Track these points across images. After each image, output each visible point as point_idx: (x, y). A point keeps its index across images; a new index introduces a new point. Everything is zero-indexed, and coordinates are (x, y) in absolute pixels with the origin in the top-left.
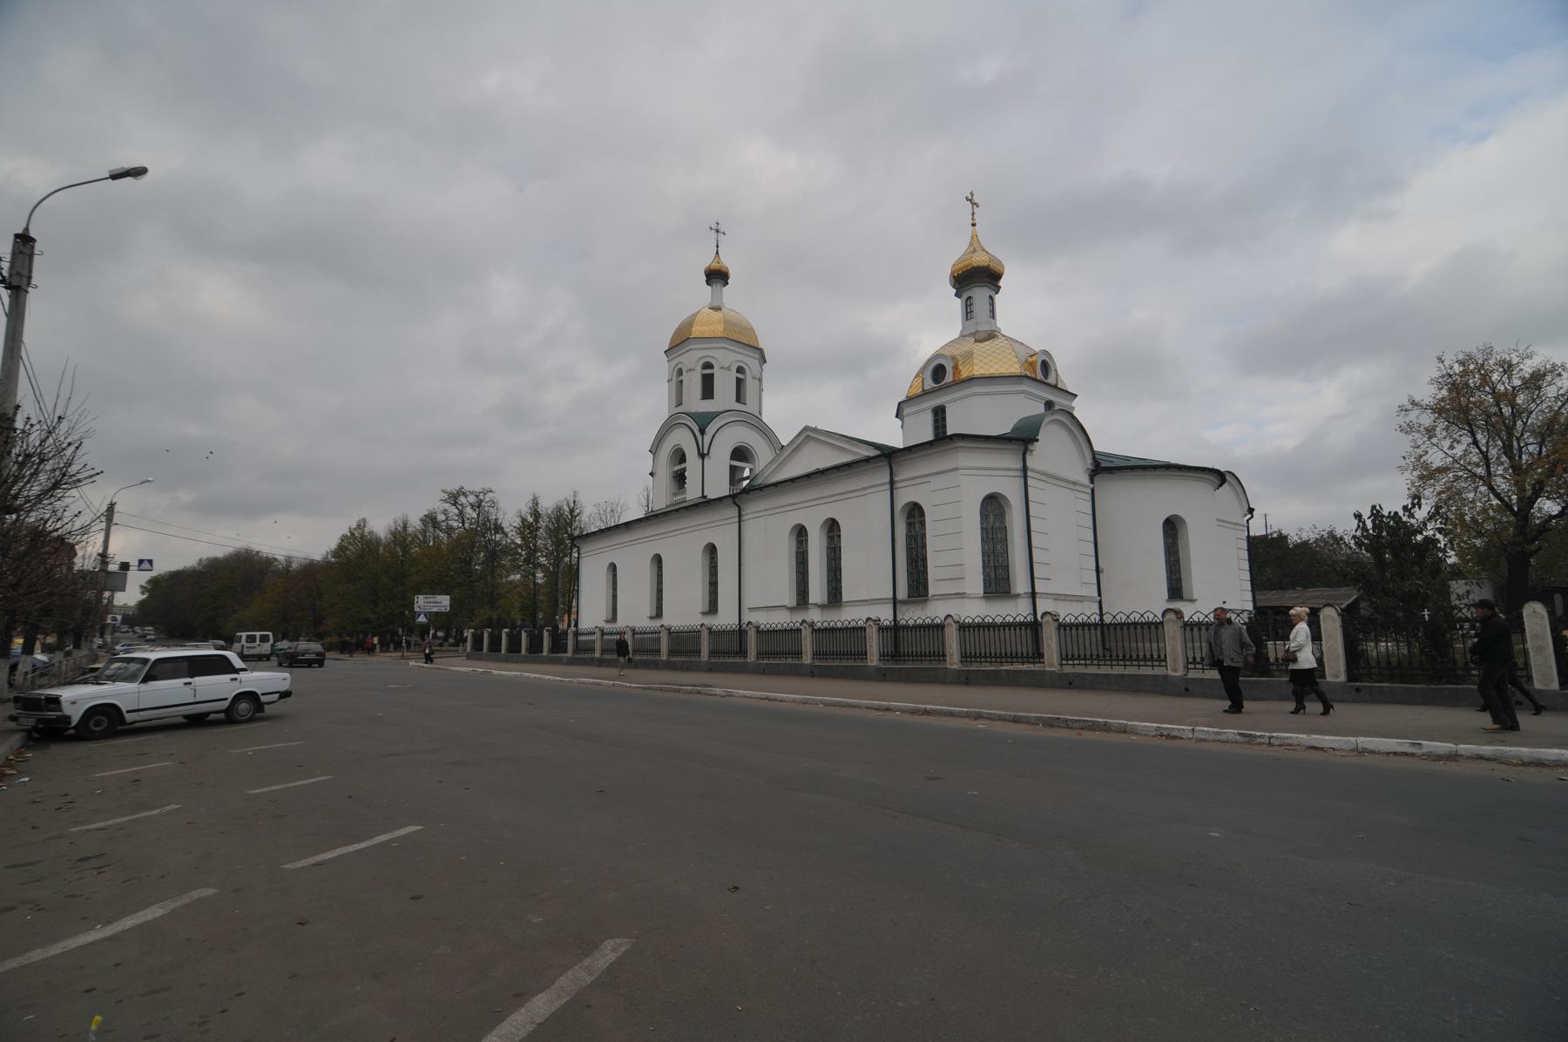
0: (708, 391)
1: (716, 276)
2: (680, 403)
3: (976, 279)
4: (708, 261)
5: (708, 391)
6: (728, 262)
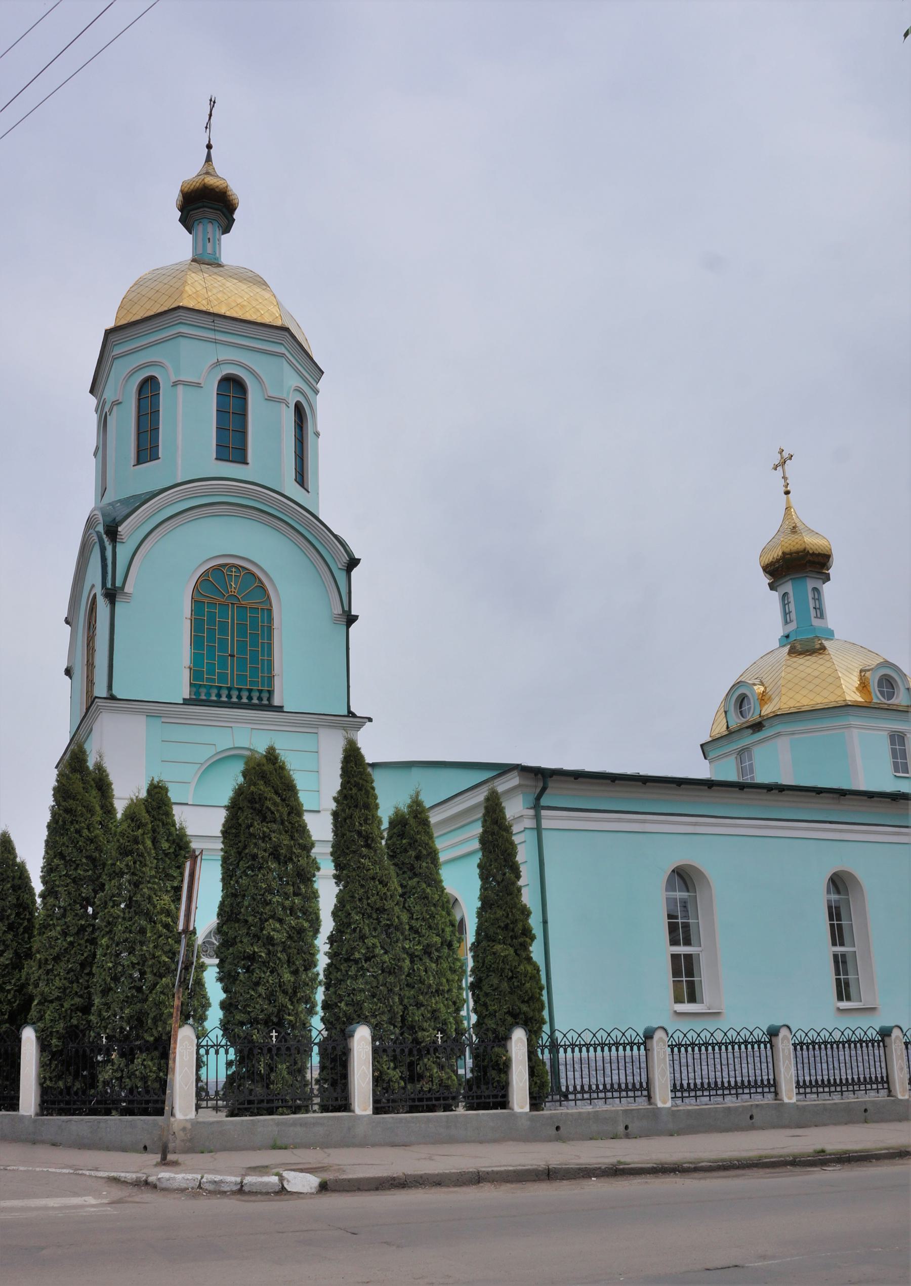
1: (207, 206)
2: (147, 449)
3: (798, 567)
4: (189, 171)
6: (230, 175)
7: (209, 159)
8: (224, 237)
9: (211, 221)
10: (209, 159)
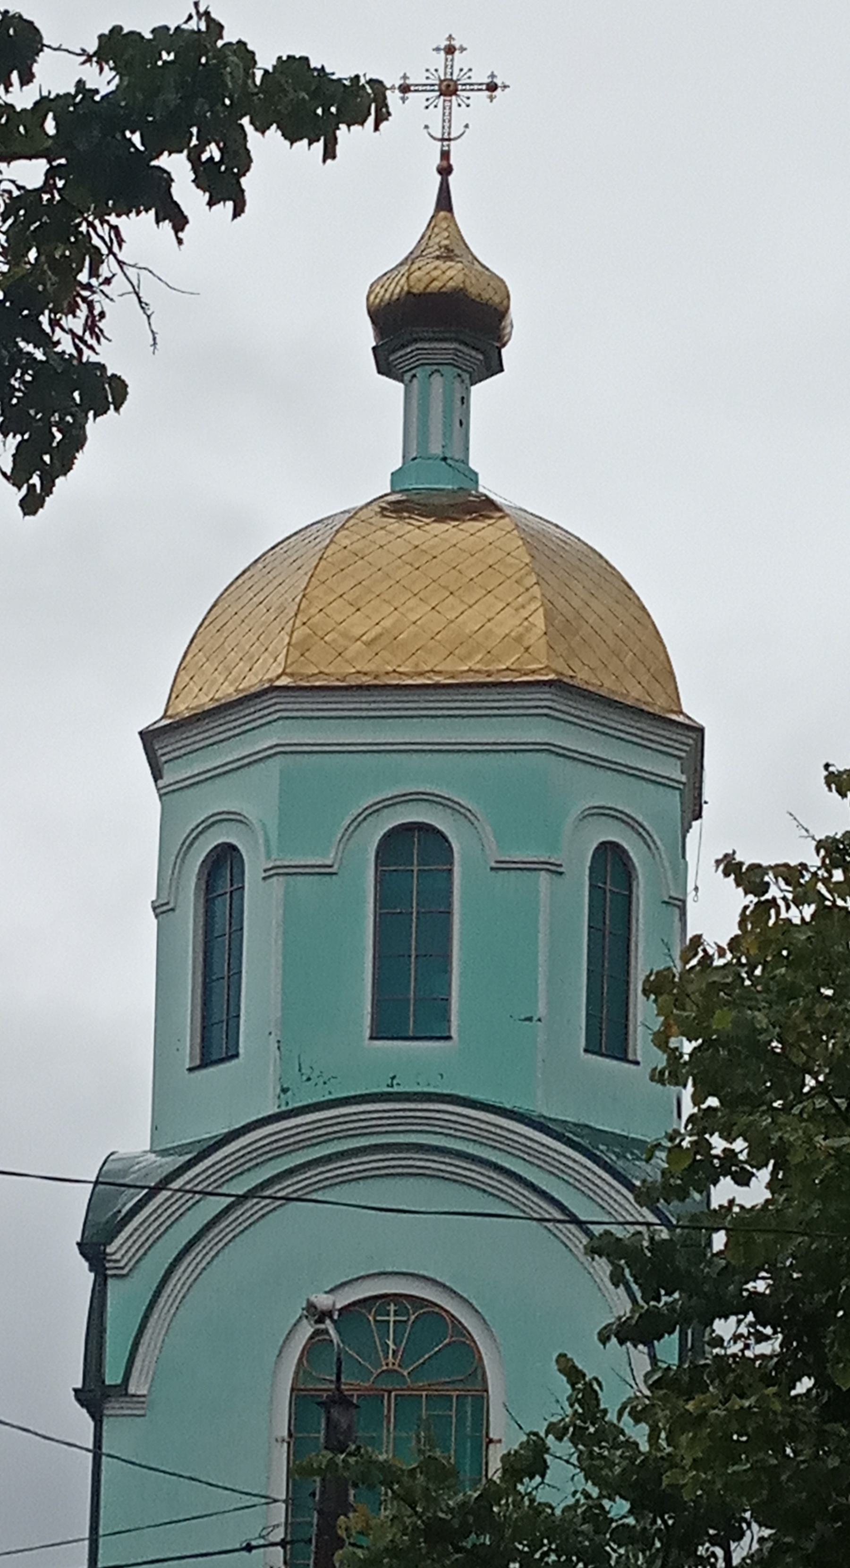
0: (409, 1000)
5: (409, 1000)
6: (494, 242)
7: (444, 201)
8: (480, 393)
9: (436, 368)
10: (444, 201)
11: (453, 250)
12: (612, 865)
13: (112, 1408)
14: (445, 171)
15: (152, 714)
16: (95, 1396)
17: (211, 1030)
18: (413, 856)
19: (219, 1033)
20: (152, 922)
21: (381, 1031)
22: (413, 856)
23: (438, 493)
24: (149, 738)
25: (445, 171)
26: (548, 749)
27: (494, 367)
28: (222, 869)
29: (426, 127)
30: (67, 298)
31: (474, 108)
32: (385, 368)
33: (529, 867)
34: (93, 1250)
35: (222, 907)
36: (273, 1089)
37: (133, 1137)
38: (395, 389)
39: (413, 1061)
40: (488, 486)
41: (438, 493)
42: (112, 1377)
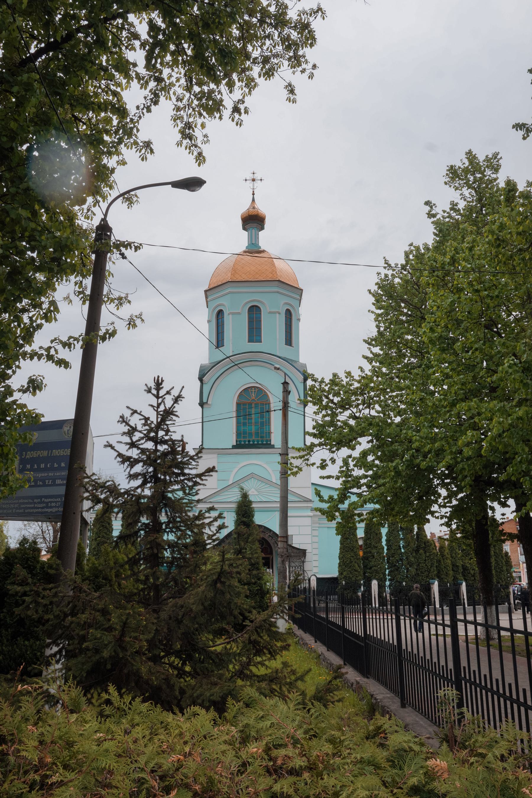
0: (254, 332)
4: (244, 207)
5: (254, 332)
6: (262, 208)
7: (253, 200)
8: (261, 233)
9: (253, 228)
10: (253, 200)
11: (254, 208)
12: (289, 314)
13: (205, 406)
14: (253, 194)
15: (206, 288)
16: (202, 404)
17: (219, 342)
18: (254, 311)
19: (220, 343)
20: (207, 325)
21: (250, 341)
22: (254, 311)
23: (254, 250)
24: (206, 291)
25: (253, 194)
26: (278, 292)
27: (262, 228)
28: (220, 314)
29: (369, 311)
30: (437, 242)
31: (258, 184)
32: (244, 228)
33: (274, 313)
34: (201, 379)
35: (220, 321)
36: (231, 351)
37: (205, 361)
38: (246, 233)
39: (255, 346)
40: (263, 248)
41: (254, 250)
42: (205, 401)
